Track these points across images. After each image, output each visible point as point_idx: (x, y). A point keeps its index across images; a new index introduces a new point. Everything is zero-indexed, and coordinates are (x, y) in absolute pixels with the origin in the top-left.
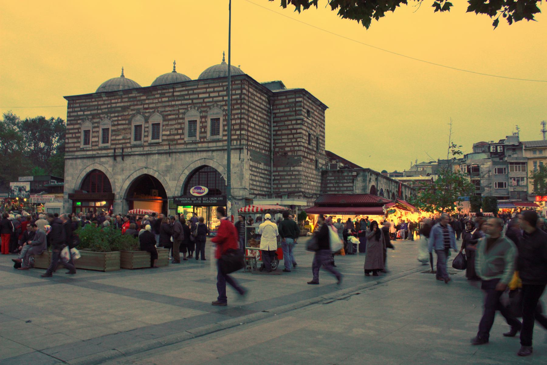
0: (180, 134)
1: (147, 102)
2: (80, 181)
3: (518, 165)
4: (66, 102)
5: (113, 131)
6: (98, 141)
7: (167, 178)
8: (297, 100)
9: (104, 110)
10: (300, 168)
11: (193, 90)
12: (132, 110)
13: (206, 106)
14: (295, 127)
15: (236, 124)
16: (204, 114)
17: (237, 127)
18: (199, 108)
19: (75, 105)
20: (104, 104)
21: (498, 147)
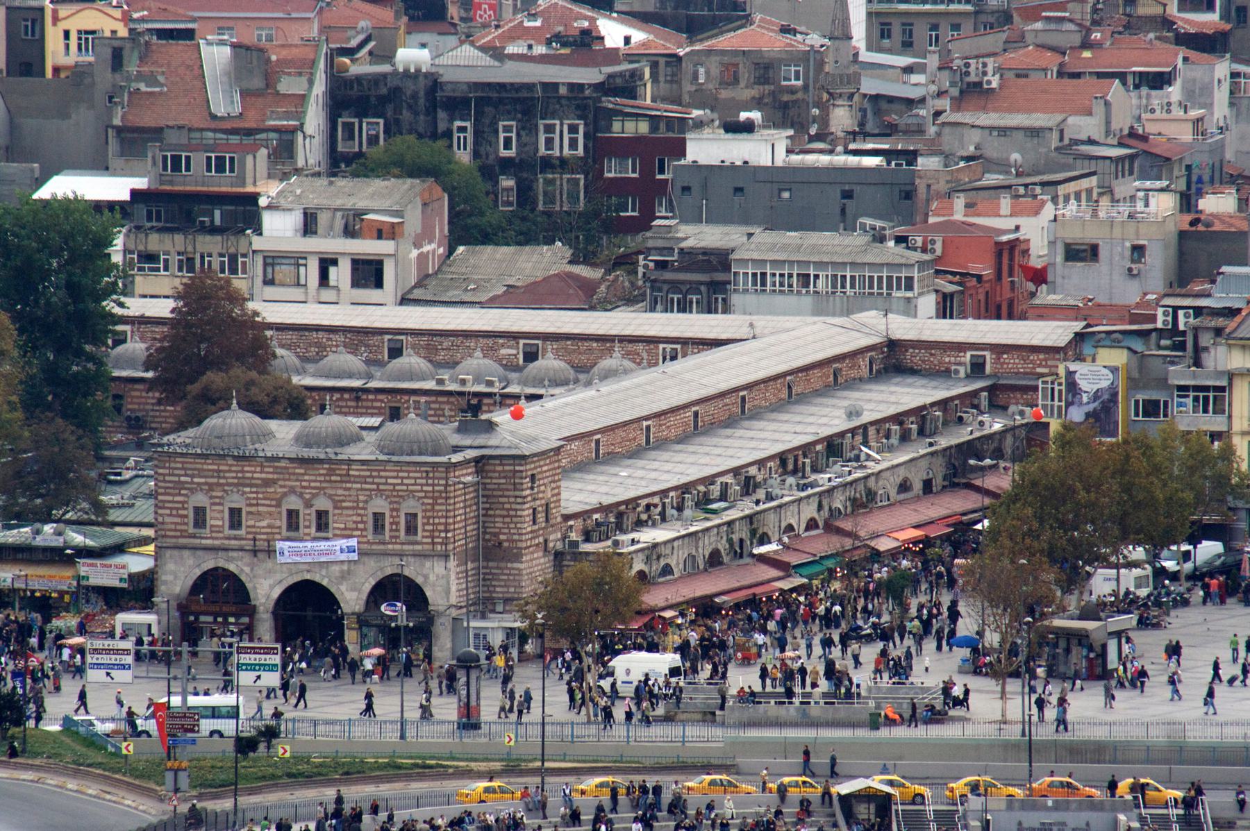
0: (361, 530)
1: (306, 478)
2: (190, 582)
3: (1201, 394)
5: (249, 513)
6: (223, 526)
7: (343, 588)
8: (517, 468)
9: (230, 481)
10: (522, 566)
11: (379, 471)
12: (281, 487)
14: (514, 506)
15: (440, 524)
16: (395, 506)
17: (442, 527)
18: (387, 497)
19: (173, 465)
20: (230, 471)
21: (1181, 313)
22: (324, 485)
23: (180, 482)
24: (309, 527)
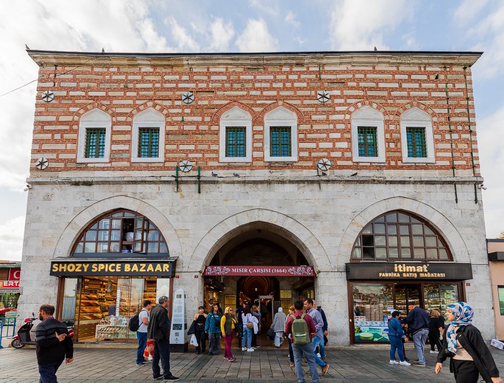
4: (33, 70)
13: (397, 106)
22: (90, 362)
23: (195, 143)
24: (261, 149)
